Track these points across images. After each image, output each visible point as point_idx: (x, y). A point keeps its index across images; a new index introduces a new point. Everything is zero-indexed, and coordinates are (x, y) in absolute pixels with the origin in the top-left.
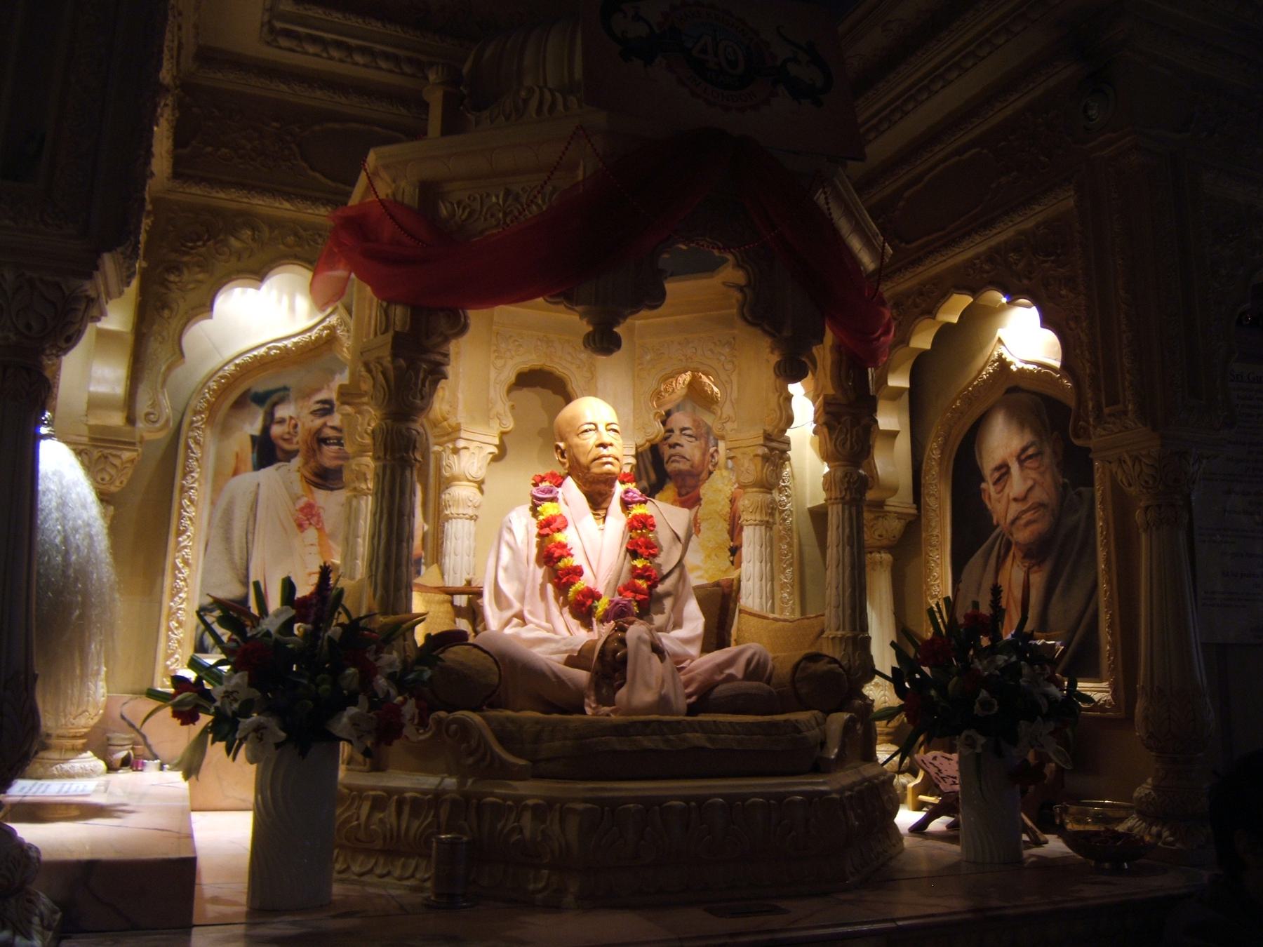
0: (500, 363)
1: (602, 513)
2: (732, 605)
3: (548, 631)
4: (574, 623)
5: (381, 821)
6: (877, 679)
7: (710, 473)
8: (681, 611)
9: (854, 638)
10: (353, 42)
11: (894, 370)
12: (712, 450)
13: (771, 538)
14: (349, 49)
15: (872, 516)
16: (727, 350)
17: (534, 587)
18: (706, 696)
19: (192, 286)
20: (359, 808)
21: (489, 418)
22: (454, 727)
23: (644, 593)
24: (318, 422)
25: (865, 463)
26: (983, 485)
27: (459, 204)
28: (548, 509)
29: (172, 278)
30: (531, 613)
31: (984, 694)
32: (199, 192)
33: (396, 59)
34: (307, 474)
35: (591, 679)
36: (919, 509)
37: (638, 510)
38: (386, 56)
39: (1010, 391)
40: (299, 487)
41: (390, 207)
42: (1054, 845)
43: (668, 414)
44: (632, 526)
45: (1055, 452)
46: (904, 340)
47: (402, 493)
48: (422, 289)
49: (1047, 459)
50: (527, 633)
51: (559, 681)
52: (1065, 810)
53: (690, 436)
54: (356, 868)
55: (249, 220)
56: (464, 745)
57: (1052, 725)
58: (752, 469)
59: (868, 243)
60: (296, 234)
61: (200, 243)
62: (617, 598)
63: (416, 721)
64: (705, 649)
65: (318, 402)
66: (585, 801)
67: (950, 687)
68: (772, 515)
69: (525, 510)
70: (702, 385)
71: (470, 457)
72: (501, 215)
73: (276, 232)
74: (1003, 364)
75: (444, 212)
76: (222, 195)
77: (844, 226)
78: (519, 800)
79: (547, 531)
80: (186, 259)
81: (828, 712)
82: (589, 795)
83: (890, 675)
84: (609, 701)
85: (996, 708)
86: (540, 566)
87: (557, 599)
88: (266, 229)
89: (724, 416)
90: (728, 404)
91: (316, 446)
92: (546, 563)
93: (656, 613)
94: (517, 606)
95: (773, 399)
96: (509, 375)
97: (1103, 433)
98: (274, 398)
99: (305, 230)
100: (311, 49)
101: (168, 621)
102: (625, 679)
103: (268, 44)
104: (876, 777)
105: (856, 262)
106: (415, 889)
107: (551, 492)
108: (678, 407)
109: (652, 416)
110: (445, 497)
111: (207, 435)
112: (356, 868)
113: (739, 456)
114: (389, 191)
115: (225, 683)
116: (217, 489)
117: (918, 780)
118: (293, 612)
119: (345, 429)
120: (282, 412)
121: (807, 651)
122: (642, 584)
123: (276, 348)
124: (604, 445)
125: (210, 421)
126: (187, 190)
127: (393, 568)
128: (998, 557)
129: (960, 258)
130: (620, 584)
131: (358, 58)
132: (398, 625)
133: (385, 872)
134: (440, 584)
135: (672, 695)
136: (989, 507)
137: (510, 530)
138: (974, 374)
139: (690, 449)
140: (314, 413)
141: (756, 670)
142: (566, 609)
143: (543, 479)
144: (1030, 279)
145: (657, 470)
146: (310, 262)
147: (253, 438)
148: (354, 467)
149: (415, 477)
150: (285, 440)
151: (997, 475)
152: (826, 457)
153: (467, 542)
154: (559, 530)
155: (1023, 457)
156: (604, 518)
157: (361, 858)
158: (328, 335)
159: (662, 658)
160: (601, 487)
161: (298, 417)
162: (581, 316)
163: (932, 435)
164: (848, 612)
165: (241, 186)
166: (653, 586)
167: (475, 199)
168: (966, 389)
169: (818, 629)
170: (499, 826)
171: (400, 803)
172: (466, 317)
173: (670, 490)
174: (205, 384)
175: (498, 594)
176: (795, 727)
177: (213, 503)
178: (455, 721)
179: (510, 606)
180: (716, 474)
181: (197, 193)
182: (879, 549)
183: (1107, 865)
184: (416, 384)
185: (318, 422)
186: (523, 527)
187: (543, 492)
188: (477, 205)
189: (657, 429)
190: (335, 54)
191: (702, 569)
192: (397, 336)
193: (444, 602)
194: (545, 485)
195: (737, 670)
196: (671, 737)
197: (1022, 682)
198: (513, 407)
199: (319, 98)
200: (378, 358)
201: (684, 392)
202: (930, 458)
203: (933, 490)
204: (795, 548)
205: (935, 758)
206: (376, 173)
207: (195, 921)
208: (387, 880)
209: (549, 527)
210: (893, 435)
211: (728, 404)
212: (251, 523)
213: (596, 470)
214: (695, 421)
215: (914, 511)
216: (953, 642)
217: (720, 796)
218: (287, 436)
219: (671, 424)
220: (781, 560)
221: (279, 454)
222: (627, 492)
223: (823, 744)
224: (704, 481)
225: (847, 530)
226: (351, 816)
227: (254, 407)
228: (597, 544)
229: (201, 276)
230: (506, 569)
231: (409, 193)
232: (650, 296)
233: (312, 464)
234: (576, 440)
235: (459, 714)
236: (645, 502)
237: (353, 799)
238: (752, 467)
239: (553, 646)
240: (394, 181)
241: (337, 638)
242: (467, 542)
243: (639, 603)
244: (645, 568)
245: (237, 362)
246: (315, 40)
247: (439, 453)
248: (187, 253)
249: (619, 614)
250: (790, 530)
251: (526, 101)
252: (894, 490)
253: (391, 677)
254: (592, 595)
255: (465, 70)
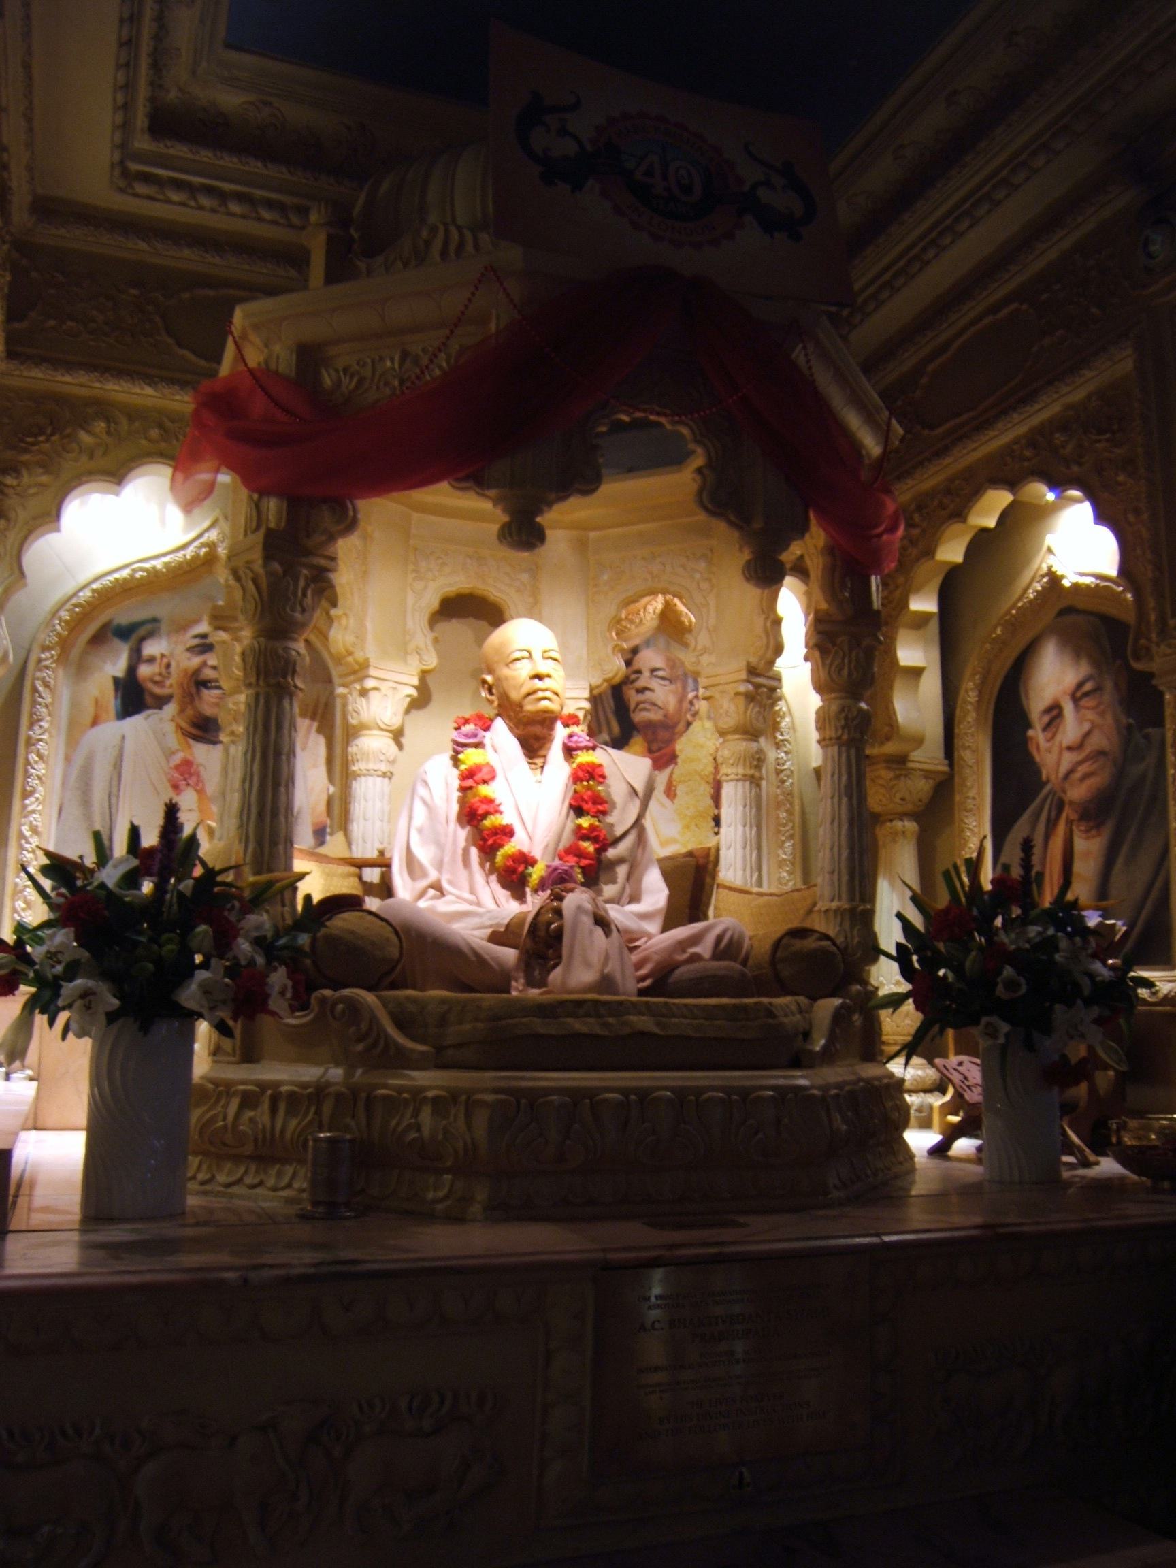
0: (419, 585)
1: (539, 761)
2: (708, 880)
3: (471, 903)
4: (503, 894)
5: (251, 1120)
6: (883, 958)
7: (689, 724)
8: (639, 882)
9: (852, 911)
10: (227, 187)
11: (918, 590)
12: (691, 695)
13: (758, 797)
14: (223, 196)
15: (891, 774)
16: (702, 565)
17: (454, 852)
18: (663, 979)
19: (32, 491)
20: (226, 1106)
21: (406, 653)
22: (340, 1006)
23: (593, 856)
24: (196, 661)
25: (868, 693)
26: (1030, 733)
27: (345, 370)
28: (471, 757)
29: (9, 480)
30: (450, 883)
31: (1008, 971)
32: (40, 375)
33: (281, 207)
34: (184, 725)
35: (519, 959)
36: (951, 765)
37: (584, 758)
38: (270, 204)
39: (1063, 612)
40: (173, 740)
41: (261, 378)
42: (1108, 1166)
43: (635, 651)
44: (576, 778)
45: (1116, 685)
46: (930, 552)
47: (279, 727)
48: (305, 474)
49: (1108, 695)
50: (444, 906)
51: (479, 961)
52: (1123, 1127)
53: (663, 678)
54: (222, 1178)
55: (102, 409)
56: (352, 1029)
57: (1096, 1011)
58: (732, 711)
59: (870, 418)
60: (161, 426)
61: (41, 438)
62: (557, 862)
63: (289, 995)
64: (666, 928)
65: (196, 637)
66: (497, 1091)
67: (968, 964)
68: (758, 767)
69: (445, 759)
70: (677, 614)
71: (381, 701)
72: (396, 383)
73: (137, 424)
74: (1054, 579)
75: (327, 381)
76: (68, 379)
77: (836, 398)
78: (417, 1092)
79: (469, 782)
80: (25, 457)
81: (814, 999)
82: (503, 1084)
83: (894, 953)
84: (542, 983)
85: (1024, 989)
86: (463, 827)
87: (482, 865)
88: (124, 422)
89: (699, 647)
90: (704, 632)
91: (193, 690)
92: (469, 822)
93: (606, 884)
94: (433, 875)
95: (759, 621)
96: (431, 600)
97: (1169, 651)
98: (142, 631)
99: (173, 421)
100: (175, 197)
101: (13, 900)
102: (560, 957)
103: (122, 190)
104: (879, 1079)
105: (855, 447)
106: (289, 1201)
107: (475, 736)
108: (647, 643)
109: (610, 649)
110: (352, 749)
111: (59, 678)
112: (222, 1178)
113: (717, 696)
114: (261, 359)
115: (48, 943)
116: (72, 741)
117: (948, 1097)
118: (135, 862)
119: (221, 667)
120: (152, 648)
121: (790, 926)
122: (589, 847)
123: (142, 570)
124: (539, 677)
125: (63, 659)
126: (26, 373)
127: (268, 819)
128: (1049, 820)
129: (994, 445)
130: (561, 847)
131: (235, 207)
132: (270, 884)
133: (256, 1181)
134: (346, 854)
135: (618, 977)
136: (1037, 758)
137: (425, 783)
138: (1019, 592)
139: (663, 695)
140: (191, 649)
141: (728, 948)
142: (493, 878)
143: (467, 722)
144: (1080, 464)
145: (618, 715)
146: (172, 458)
147: (116, 681)
148: (231, 706)
149: (297, 710)
150: (156, 683)
151: (1046, 719)
152: (819, 687)
153: (378, 805)
154: (485, 782)
155: (1079, 694)
156: (542, 767)
157: (228, 1166)
158: (206, 554)
159: (608, 933)
160: (537, 729)
161: (172, 654)
162: (496, 502)
163: (968, 672)
164: (845, 878)
165: (91, 367)
166: (602, 849)
167: (365, 364)
168: (1008, 612)
169: (809, 902)
170: (394, 1123)
171: (275, 1100)
172: (355, 510)
173: (638, 742)
174: (55, 614)
175: (412, 863)
176: (769, 1012)
177: (68, 759)
178: (343, 999)
179: (424, 874)
180: (696, 726)
181: (37, 377)
182: (902, 816)
183: (1166, 1185)
184: (295, 594)
185: (196, 661)
186: (442, 783)
187: (466, 736)
188: (367, 372)
189: (616, 666)
190: (205, 201)
191: (669, 834)
192: (270, 534)
193: (349, 875)
194: (469, 728)
195: (704, 949)
196: (611, 1020)
197: (1058, 957)
198: (436, 641)
199: (187, 259)
200: (247, 562)
201: (655, 623)
202: (965, 702)
203: (968, 741)
204: (797, 819)
205: (960, 1064)
206: (244, 336)
207: (12, 1228)
208: (258, 1191)
209: (472, 778)
210: (916, 673)
211: (704, 632)
212: (115, 783)
213: (529, 707)
214: (668, 660)
215: (946, 769)
216: (975, 912)
217: (666, 1088)
218: (157, 678)
219: (636, 665)
220: (779, 832)
221: (149, 700)
222: (570, 736)
223: (807, 1035)
224: (681, 734)
225: (844, 778)
226: (215, 1116)
227: (117, 643)
228: (534, 802)
229: (44, 479)
230: (420, 831)
231: (284, 359)
232: (579, 477)
233: (190, 712)
234: (505, 672)
235: (346, 992)
236: (594, 748)
237: (220, 1093)
238: (732, 708)
239: (476, 921)
240: (266, 346)
241: (188, 894)
242: (378, 805)
243: (584, 870)
244: (592, 828)
245: (94, 586)
246: (179, 185)
247: (344, 697)
248: (26, 451)
249: (557, 882)
250: (790, 794)
251: (428, 243)
252: (918, 741)
253: (259, 942)
254: (525, 860)
255: (357, 210)
